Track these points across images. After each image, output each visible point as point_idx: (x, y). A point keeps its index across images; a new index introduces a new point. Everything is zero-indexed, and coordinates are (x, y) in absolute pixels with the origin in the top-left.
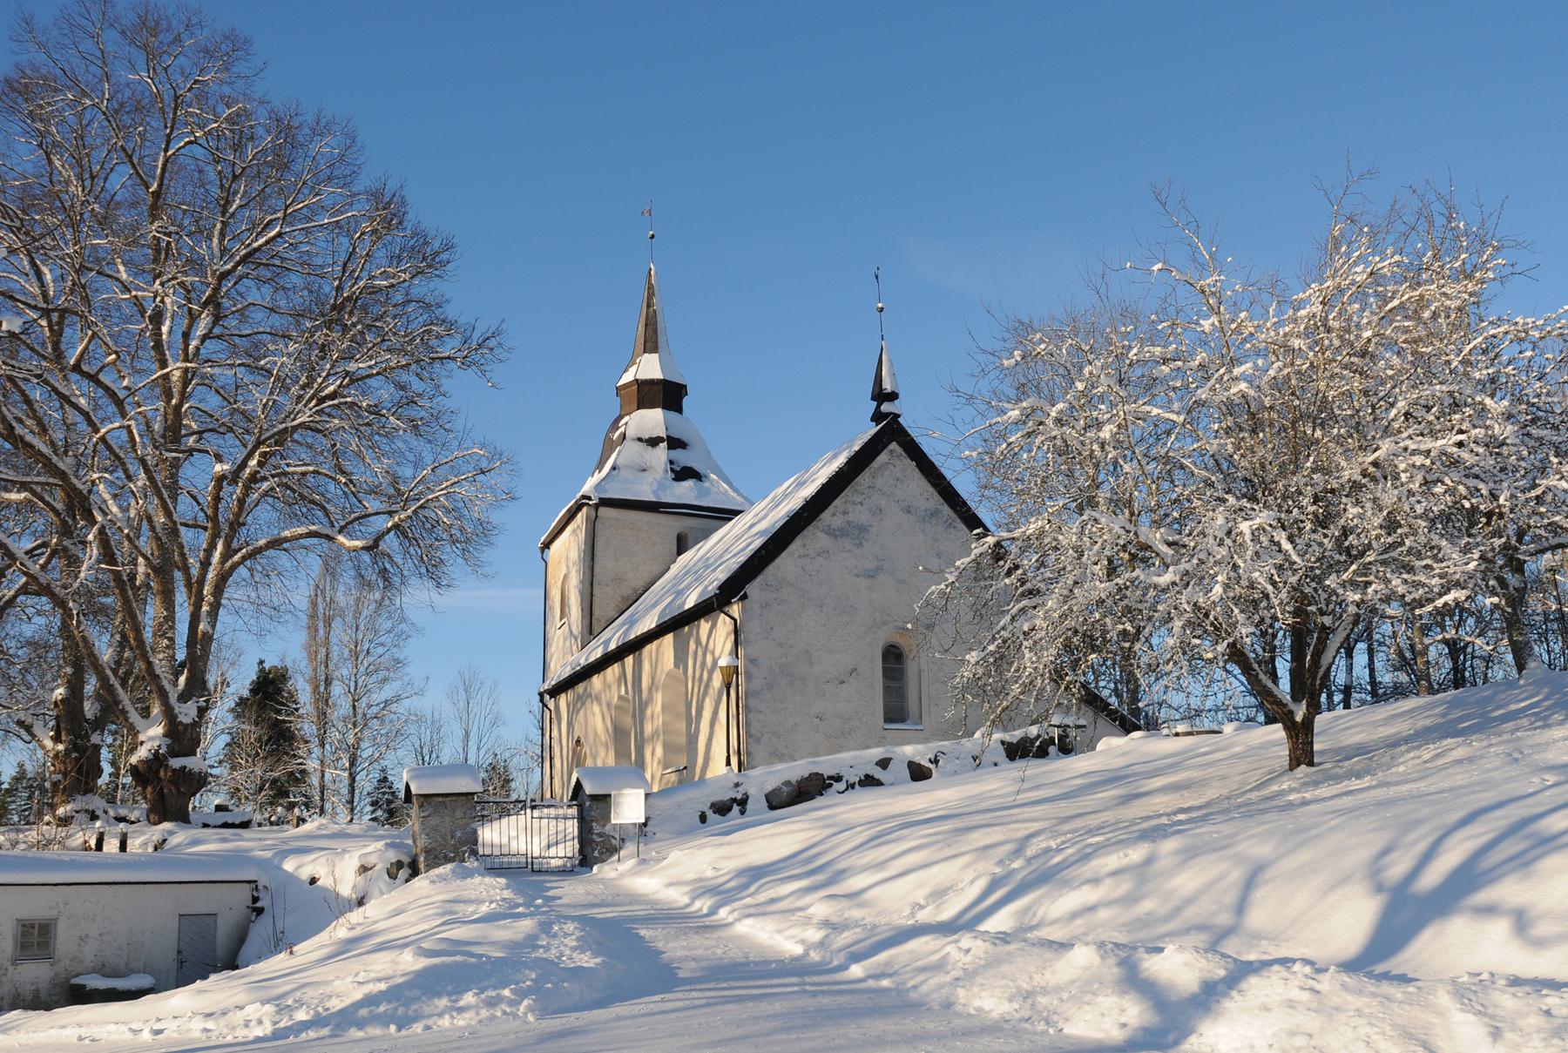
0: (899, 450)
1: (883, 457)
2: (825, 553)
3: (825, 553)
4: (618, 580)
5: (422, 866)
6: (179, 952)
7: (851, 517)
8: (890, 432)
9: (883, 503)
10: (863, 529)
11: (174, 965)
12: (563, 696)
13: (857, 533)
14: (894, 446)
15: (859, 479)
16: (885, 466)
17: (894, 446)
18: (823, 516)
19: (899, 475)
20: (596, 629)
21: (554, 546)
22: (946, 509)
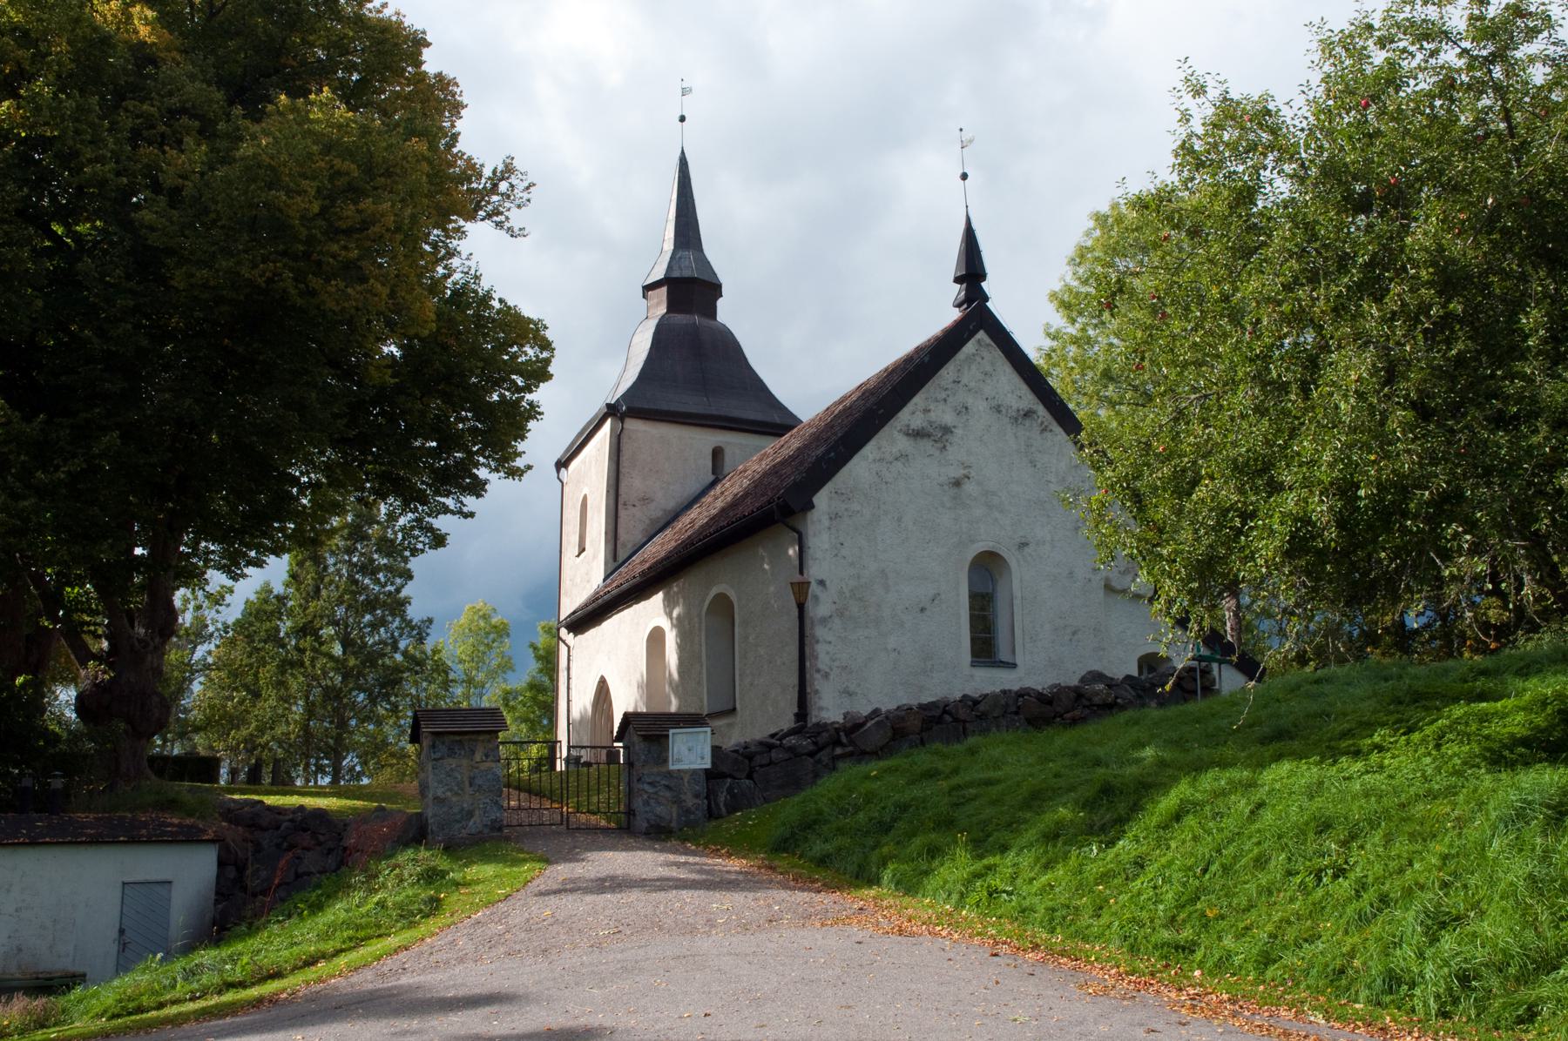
0: (988, 340)
1: (969, 348)
2: (903, 457)
3: (903, 457)
4: (646, 500)
5: (267, 780)
6: (122, 932)
7: (933, 416)
8: (977, 318)
9: (970, 401)
10: (947, 430)
11: (114, 948)
12: (485, 704)
13: (935, 435)
14: (981, 335)
15: (943, 372)
16: (970, 359)
17: (981, 335)
18: (900, 414)
19: (988, 368)
20: (622, 556)
21: (574, 464)
22: (1041, 410)
